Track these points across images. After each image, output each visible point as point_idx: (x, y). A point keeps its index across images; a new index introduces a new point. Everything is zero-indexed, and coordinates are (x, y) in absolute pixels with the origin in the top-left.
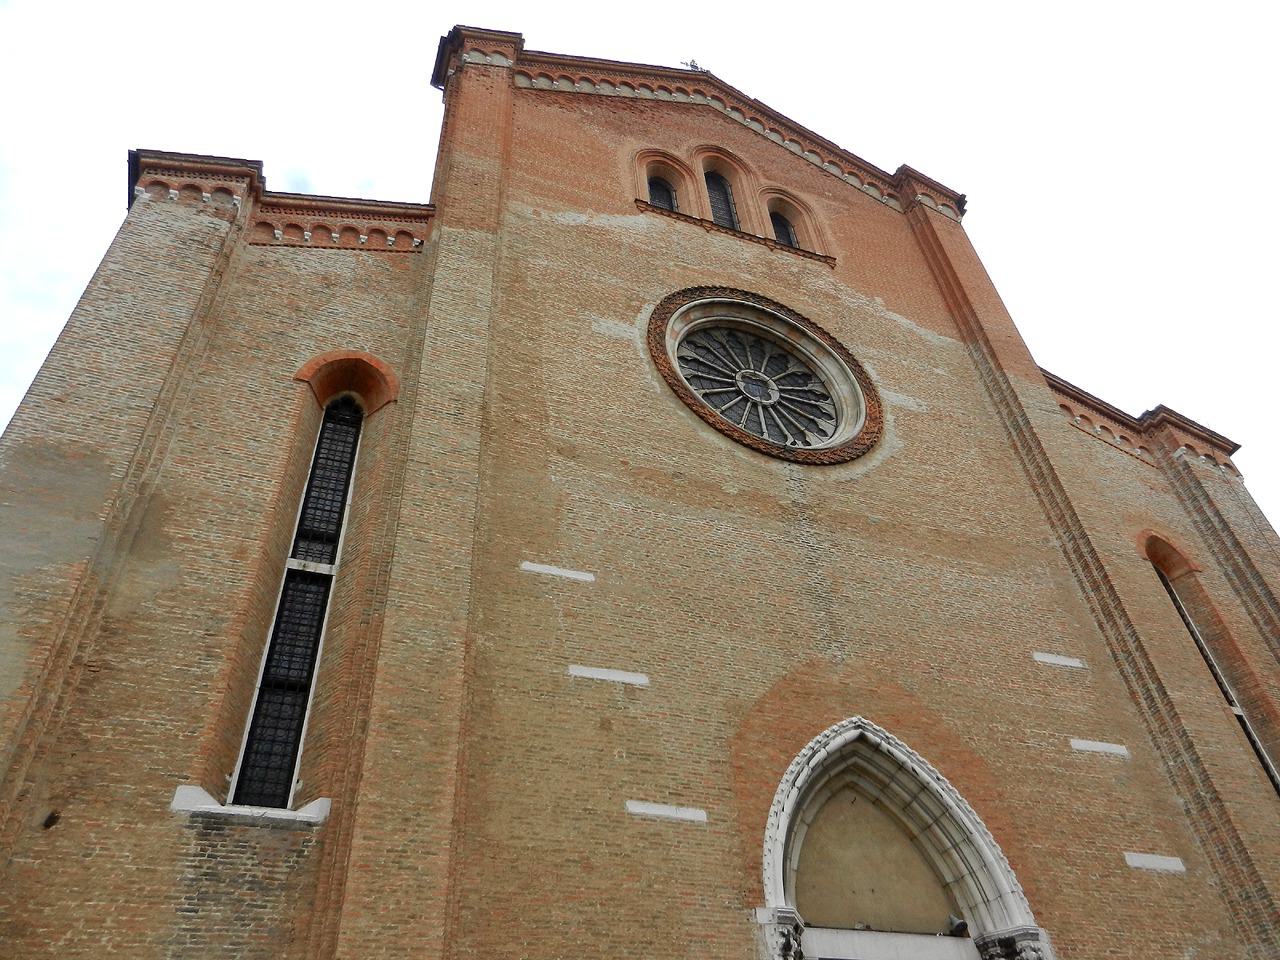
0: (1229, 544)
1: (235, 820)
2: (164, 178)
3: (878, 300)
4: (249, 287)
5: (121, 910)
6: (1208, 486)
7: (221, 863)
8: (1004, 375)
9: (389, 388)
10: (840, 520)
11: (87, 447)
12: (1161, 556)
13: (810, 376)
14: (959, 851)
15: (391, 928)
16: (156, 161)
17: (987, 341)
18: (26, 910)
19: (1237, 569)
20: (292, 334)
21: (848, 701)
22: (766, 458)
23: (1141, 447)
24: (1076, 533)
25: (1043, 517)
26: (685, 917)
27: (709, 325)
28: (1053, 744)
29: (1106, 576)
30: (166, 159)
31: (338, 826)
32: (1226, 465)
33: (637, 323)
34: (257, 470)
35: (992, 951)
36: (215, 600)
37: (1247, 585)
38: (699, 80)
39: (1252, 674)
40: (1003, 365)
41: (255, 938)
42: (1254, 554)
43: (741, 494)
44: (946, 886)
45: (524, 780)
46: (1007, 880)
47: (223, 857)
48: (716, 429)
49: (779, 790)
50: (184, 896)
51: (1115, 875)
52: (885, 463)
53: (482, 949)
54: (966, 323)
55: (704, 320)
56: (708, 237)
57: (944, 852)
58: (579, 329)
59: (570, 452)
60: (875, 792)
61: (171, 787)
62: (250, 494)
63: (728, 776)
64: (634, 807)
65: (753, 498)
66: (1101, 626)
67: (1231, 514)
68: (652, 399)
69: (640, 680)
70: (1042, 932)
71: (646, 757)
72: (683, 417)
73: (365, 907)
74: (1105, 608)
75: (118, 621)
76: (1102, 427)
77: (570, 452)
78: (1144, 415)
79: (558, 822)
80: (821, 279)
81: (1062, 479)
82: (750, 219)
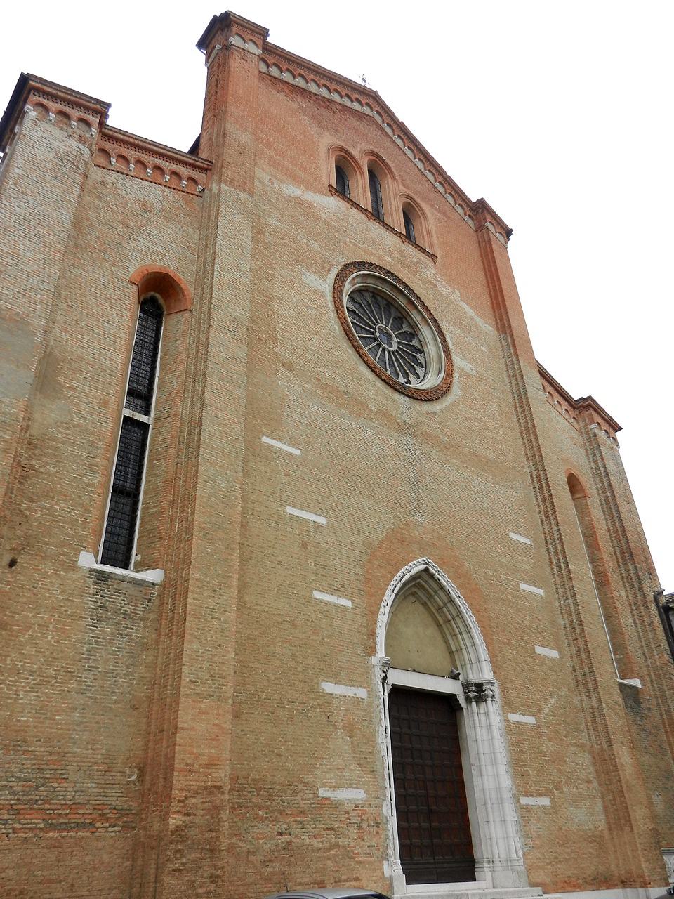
0: (606, 485)
1: (113, 576)
2: (45, 102)
3: (457, 292)
4: (97, 201)
5: (58, 621)
6: (603, 448)
7: (108, 601)
8: (518, 360)
9: (186, 299)
10: (427, 437)
11: (18, 314)
12: (573, 483)
13: (413, 335)
14: (462, 636)
15: (209, 651)
16: (40, 86)
17: (512, 335)
18: (5, 615)
19: (607, 500)
20: (126, 246)
21: (423, 548)
22: (392, 390)
23: (574, 418)
24: (540, 467)
25: (523, 453)
26: (339, 658)
27: (363, 288)
28: (512, 585)
29: (551, 495)
30: (47, 86)
31: (175, 589)
32: (613, 438)
33: (327, 280)
34: (110, 346)
35: (470, 688)
36: (93, 434)
38: (373, 98)
39: (602, 558)
40: (519, 353)
41: (129, 645)
42: (617, 493)
43: (378, 411)
44: (451, 653)
45: (263, 573)
46: (484, 654)
47: (109, 597)
48: (368, 366)
49: (386, 594)
50: (89, 617)
51: (530, 657)
52: (451, 404)
53: (242, 664)
54: (501, 319)
55: (362, 285)
56: (369, 223)
57: (455, 635)
58: (295, 278)
59: (288, 366)
60: (424, 598)
61: (77, 552)
62: (108, 363)
63: (363, 583)
64: (317, 595)
65: (384, 414)
66: (542, 522)
67: (611, 469)
68: (334, 338)
69: (322, 520)
70: (496, 682)
71: (324, 567)
72: (350, 354)
73: (196, 638)
74: (546, 512)
75: (37, 439)
76: (558, 401)
77: (288, 366)
78: (580, 399)
79: (279, 598)
80: (429, 271)
81: (538, 433)
82: (392, 215)
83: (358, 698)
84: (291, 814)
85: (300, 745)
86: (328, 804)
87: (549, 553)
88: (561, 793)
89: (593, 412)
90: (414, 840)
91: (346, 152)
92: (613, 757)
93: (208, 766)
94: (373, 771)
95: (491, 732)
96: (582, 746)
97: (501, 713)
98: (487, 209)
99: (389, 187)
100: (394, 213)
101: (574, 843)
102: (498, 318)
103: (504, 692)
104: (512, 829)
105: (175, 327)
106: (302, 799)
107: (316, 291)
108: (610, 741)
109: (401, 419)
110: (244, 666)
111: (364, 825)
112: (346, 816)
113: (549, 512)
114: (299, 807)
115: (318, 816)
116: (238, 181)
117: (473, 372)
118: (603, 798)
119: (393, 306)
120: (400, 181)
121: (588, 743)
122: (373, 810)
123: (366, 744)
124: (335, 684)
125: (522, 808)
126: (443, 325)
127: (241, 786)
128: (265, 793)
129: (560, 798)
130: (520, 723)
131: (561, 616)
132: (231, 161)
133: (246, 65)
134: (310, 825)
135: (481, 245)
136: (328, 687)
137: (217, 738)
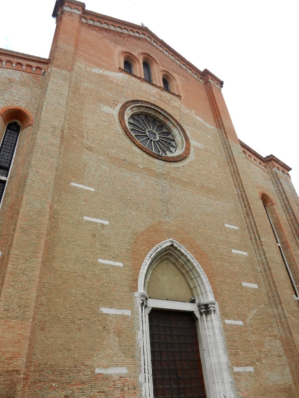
3: (193, 112)
6: (281, 180)
8: (228, 140)
10: (173, 179)
12: (265, 199)
15: (19, 292)
17: (224, 129)
19: (285, 205)
21: (169, 234)
22: (153, 158)
23: (264, 166)
24: (242, 190)
27: (139, 113)
28: (227, 251)
29: (249, 203)
32: (287, 174)
33: (116, 109)
37: (287, 210)
38: (144, 30)
39: (284, 235)
40: (228, 137)
42: (291, 201)
44: (191, 289)
46: (208, 288)
51: (238, 288)
52: (189, 163)
53: (49, 300)
54: (219, 122)
55: (138, 111)
56: (142, 84)
57: (192, 279)
59: (90, 149)
60: (174, 261)
64: (100, 261)
65: (148, 170)
67: (286, 188)
69: (106, 223)
70: (216, 302)
71: (106, 246)
73: (11, 286)
74: (247, 213)
77: (90, 149)
80: (176, 102)
81: (240, 173)
83: (125, 315)
84: (75, 384)
85: (84, 343)
86: (101, 377)
87: (250, 233)
88: (261, 363)
89: (273, 162)
90: (166, 396)
91: (130, 54)
92: (293, 341)
93: (11, 358)
94: (133, 357)
95: (214, 331)
96: (275, 336)
97: (220, 320)
98: (208, 73)
99: (154, 68)
100: (157, 79)
101: (271, 393)
102: (217, 122)
103: (222, 308)
104: (228, 387)
105: (25, 135)
106: (83, 375)
107: (109, 114)
108: (291, 332)
109: (158, 171)
110: (50, 301)
111: (126, 389)
112: (113, 383)
113: (249, 213)
114: (81, 380)
115: (93, 384)
116: (62, 66)
117: (203, 147)
118: (290, 366)
119: (165, 126)
120: (160, 65)
121: (279, 334)
122: (132, 379)
123: (129, 341)
124: (110, 308)
125: (234, 373)
126: (184, 127)
127: (42, 369)
128: (58, 373)
129: (260, 367)
130: (233, 325)
131: (258, 265)
132: (59, 57)
133: (72, 18)
134: (88, 390)
135: (207, 90)
136: (105, 310)
137: (19, 342)
